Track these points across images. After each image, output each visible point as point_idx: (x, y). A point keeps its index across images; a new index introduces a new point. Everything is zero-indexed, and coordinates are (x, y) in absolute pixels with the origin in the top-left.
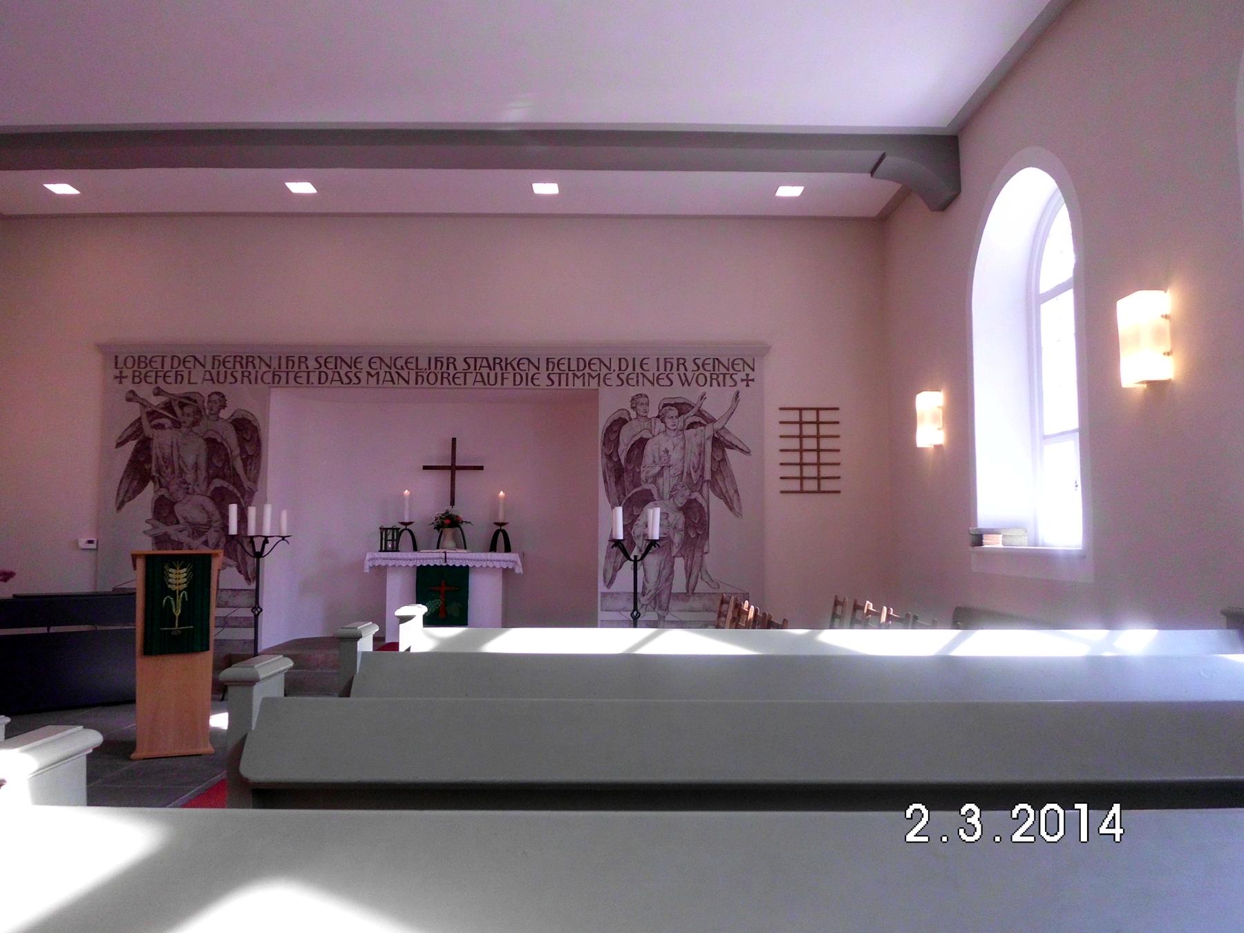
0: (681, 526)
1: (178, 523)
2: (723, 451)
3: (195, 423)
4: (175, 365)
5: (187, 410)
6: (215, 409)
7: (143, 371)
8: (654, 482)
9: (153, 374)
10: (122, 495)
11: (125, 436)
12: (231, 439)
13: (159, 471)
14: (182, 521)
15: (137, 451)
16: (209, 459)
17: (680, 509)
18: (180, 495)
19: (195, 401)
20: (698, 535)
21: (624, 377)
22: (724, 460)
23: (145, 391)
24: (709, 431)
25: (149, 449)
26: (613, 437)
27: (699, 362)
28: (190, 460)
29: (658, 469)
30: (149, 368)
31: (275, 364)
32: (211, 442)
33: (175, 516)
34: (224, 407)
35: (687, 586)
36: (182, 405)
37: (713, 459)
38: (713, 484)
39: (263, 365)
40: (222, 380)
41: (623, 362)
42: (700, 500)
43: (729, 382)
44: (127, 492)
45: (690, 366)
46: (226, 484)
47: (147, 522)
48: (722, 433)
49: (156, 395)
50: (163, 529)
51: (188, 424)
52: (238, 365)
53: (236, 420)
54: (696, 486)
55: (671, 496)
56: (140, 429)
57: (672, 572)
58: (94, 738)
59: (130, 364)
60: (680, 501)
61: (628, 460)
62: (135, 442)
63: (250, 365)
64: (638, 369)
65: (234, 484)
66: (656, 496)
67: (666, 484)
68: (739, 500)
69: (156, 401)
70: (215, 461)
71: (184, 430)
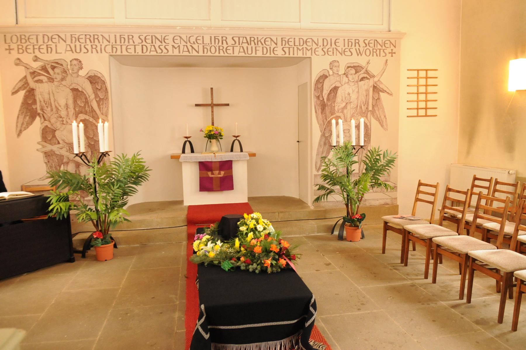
1: (59, 143)
2: (379, 93)
3: (63, 79)
4: (46, 41)
5: (56, 70)
6: (75, 71)
7: (25, 45)
8: (342, 112)
9: (31, 47)
10: (19, 125)
11: (17, 88)
12: (88, 89)
13: (42, 109)
14: (61, 142)
15: (26, 97)
16: (75, 101)
18: (58, 125)
19: (62, 65)
21: (325, 50)
22: (379, 99)
23: (27, 58)
24: (371, 82)
25: (34, 95)
27: (367, 42)
28: (62, 102)
29: (344, 104)
30: (28, 43)
31: (112, 40)
32: (75, 90)
33: (57, 139)
34: (81, 68)
36: (53, 68)
37: (373, 98)
38: (373, 112)
39: (104, 40)
40: (78, 50)
43: (382, 54)
44: (23, 124)
46: (87, 117)
47: (39, 143)
48: (378, 83)
49: (35, 61)
50: (49, 147)
51: (59, 79)
52: (88, 41)
53: (89, 77)
56: (27, 83)
59: (15, 39)
61: (328, 99)
62: (24, 92)
63: (96, 40)
64: (333, 46)
65: (93, 117)
68: (386, 121)
69: (36, 66)
70: (79, 102)
71: (56, 83)
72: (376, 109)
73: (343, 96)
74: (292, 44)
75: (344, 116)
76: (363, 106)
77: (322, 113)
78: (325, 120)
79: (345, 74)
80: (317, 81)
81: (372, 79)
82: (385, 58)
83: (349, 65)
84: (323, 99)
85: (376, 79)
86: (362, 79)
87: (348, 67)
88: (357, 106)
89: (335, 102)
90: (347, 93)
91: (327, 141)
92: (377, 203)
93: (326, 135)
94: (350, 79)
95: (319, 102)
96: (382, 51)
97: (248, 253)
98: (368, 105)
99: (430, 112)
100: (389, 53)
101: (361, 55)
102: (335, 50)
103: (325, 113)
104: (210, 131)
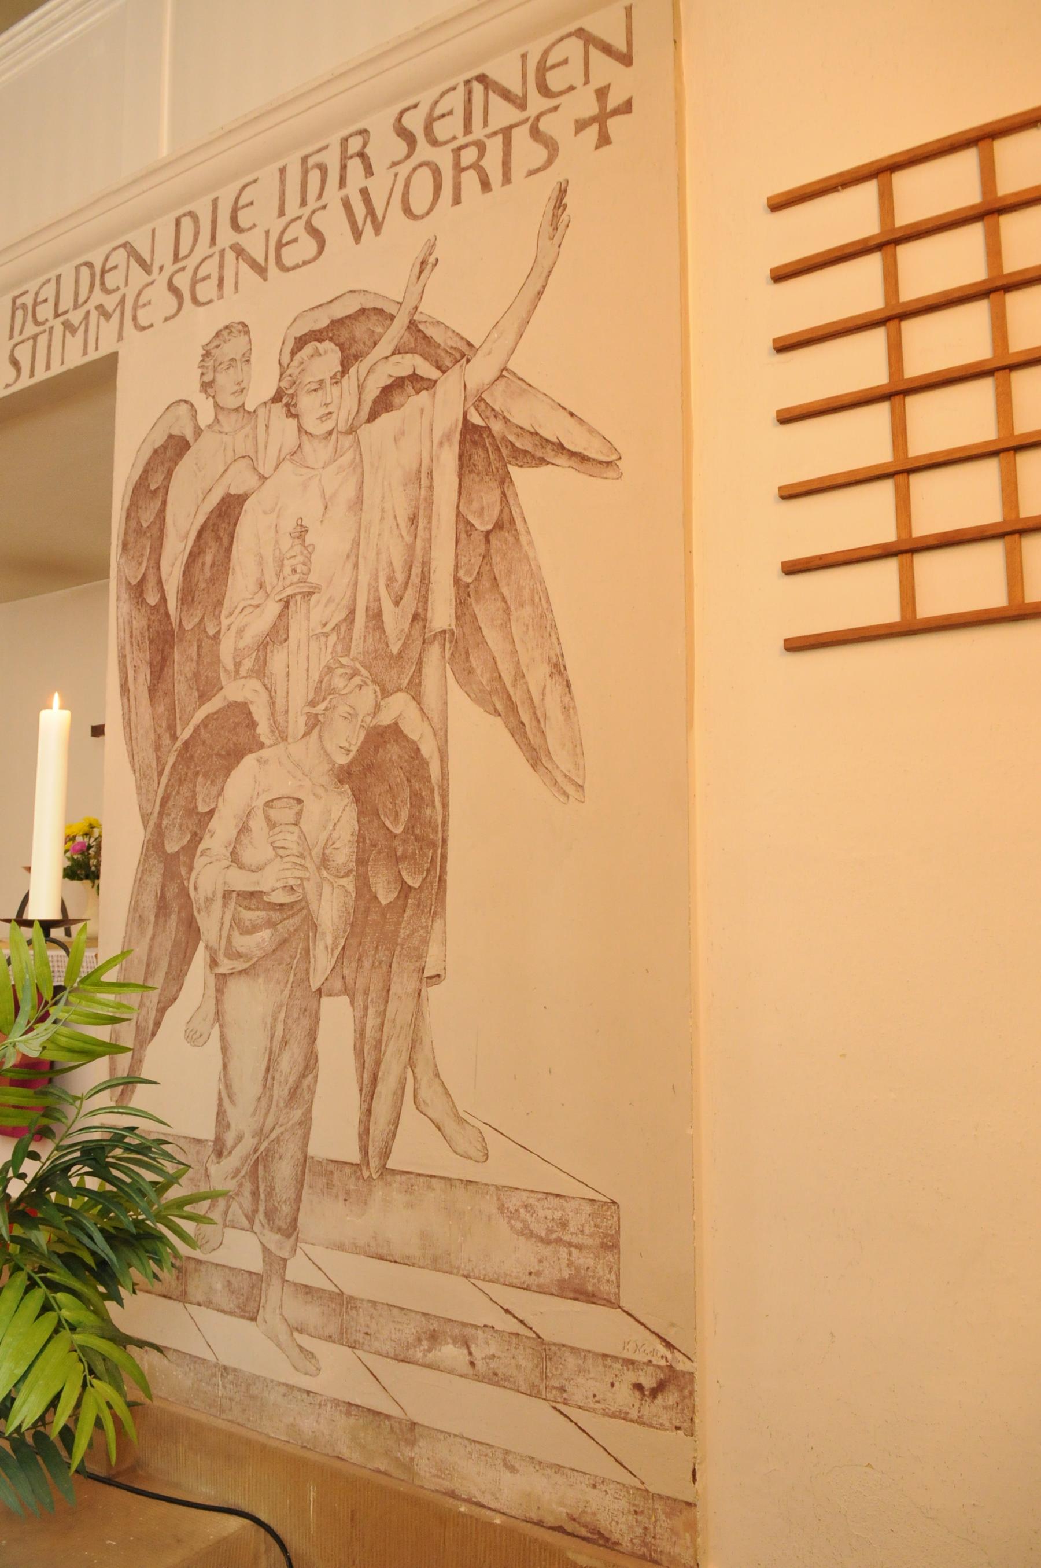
0: (343, 855)
2: (505, 480)
8: (260, 671)
20: (405, 890)
21: (182, 281)
22: (505, 523)
24: (444, 408)
26: (147, 517)
27: (414, 122)
29: (273, 609)
35: (364, 1134)
37: (464, 525)
38: (462, 643)
41: (187, 223)
42: (414, 728)
43: (527, 152)
45: (385, 147)
48: (497, 400)
54: (395, 668)
55: (314, 723)
57: (310, 1063)
60: (344, 740)
61: (187, 596)
64: (226, 236)
66: (263, 729)
67: (297, 667)
68: (568, 710)
72: (484, 611)
74: (45, 312)
75: (272, 703)
76: (387, 605)
77: (152, 691)
78: (166, 740)
79: (277, 398)
80: (136, 489)
81: (454, 374)
82: (546, 185)
83: (301, 329)
84: (164, 599)
85: (480, 371)
86: (384, 401)
87: (301, 342)
88: (352, 612)
89: (220, 603)
90: (288, 525)
91: (172, 890)
92: (504, 1491)
93: (171, 847)
94: (311, 424)
95: (140, 623)
96: (521, 136)
97: (363, 887)
98: (424, 598)
99: (855, 214)
100: (581, 126)
101: (378, 228)
102: (230, 256)
103: (170, 693)
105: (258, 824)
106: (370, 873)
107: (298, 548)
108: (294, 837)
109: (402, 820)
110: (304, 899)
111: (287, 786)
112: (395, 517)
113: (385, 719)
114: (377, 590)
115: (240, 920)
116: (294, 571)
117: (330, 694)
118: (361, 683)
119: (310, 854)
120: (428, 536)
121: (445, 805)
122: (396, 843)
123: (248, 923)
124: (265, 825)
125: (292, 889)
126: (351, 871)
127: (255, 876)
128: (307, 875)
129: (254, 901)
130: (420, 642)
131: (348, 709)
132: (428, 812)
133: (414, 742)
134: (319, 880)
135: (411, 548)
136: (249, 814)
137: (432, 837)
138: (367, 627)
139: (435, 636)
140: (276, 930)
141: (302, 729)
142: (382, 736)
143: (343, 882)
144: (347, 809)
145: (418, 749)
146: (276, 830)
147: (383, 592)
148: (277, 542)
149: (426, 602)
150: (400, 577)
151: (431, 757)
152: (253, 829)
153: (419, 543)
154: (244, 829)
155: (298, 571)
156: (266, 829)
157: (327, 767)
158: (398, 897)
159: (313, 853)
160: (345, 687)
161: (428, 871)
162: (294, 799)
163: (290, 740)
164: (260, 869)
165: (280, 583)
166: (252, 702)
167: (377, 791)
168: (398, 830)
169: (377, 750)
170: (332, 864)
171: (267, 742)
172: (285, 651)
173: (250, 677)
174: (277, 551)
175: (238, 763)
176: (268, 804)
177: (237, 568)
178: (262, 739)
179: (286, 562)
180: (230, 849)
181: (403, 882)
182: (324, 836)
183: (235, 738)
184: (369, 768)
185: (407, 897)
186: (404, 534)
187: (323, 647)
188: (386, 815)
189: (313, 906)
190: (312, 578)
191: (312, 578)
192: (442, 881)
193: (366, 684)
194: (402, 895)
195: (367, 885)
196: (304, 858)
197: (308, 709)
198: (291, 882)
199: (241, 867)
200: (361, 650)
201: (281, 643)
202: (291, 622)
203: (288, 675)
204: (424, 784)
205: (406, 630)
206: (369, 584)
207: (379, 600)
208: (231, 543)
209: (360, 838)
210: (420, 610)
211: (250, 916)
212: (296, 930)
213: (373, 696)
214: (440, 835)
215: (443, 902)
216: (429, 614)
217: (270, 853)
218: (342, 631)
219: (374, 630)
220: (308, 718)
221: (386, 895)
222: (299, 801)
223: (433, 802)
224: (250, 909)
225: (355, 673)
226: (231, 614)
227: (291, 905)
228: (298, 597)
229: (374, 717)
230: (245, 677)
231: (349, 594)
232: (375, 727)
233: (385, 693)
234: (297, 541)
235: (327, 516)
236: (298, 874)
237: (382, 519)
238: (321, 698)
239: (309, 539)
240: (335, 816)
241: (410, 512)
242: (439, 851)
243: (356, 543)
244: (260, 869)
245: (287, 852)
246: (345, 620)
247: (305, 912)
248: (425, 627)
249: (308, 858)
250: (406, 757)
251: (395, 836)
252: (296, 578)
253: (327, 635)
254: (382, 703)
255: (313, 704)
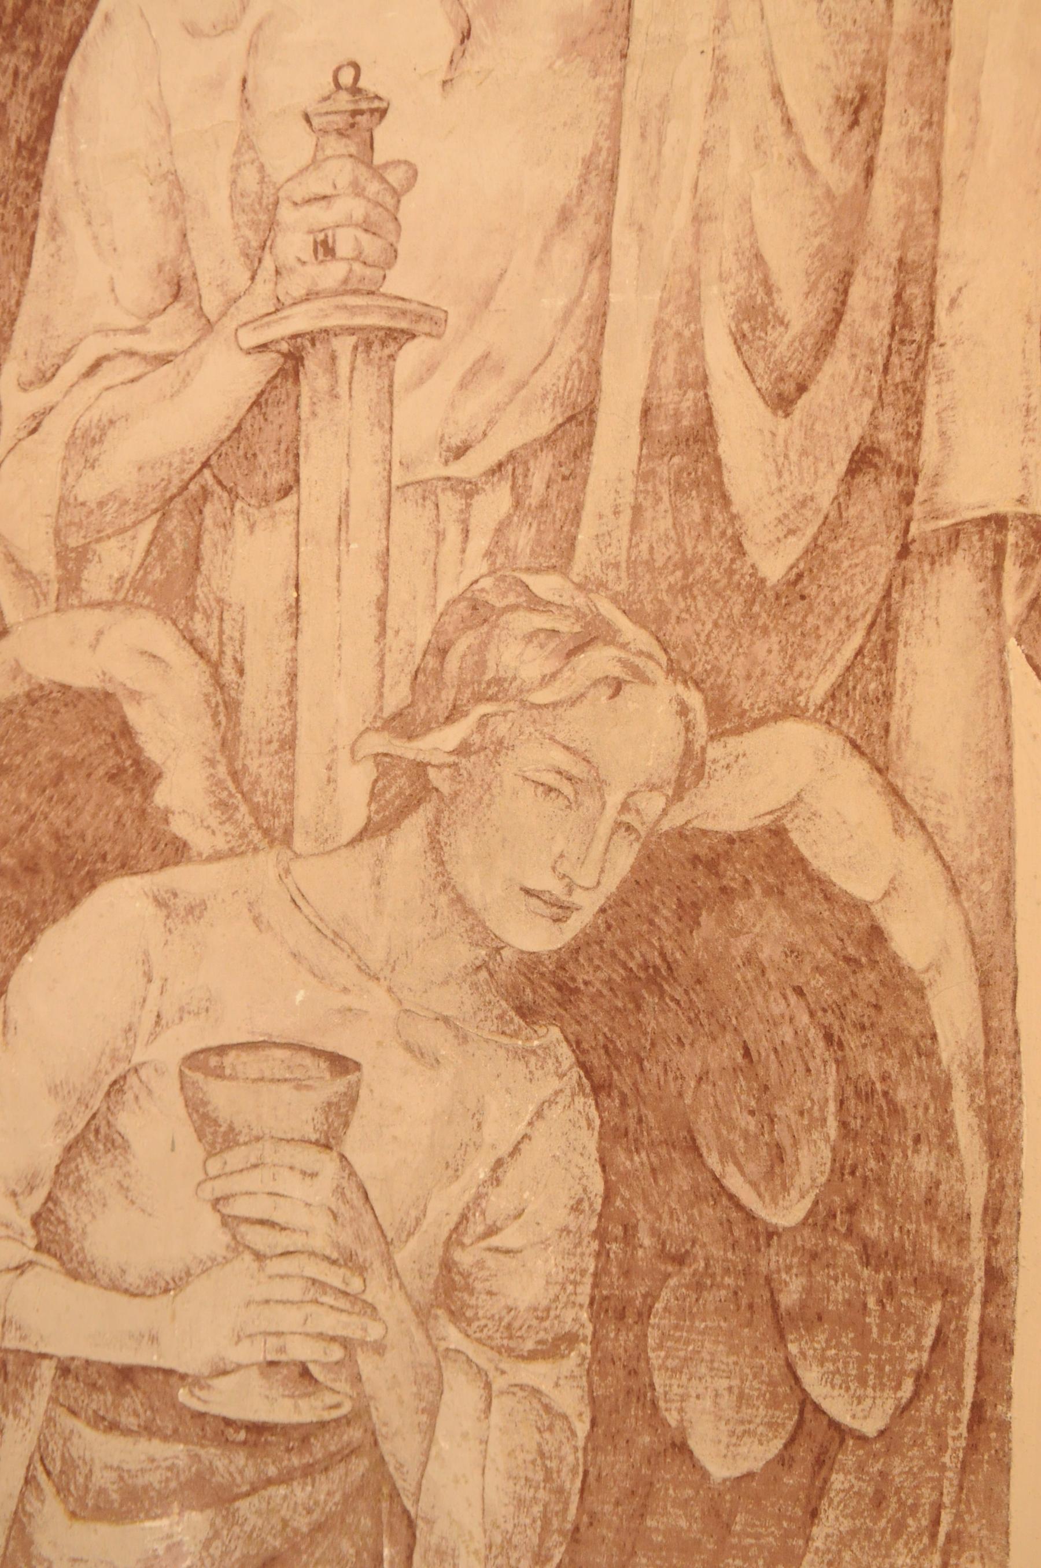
0: (536, 1271)
8: (175, 586)
17: (539, 992)
20: (816, 1440)
29: (224, 380)
42: (852, 841)
55: (404, 795)
58: (359, 1350)
60: (542, 868)
66: (183, 792)
67: (338, 595)
73: (211, 180)
75: (225, 706)
88: (580, 419)
90: (298, 81)
97: (624, 1398)
104: (280, 733)
105: (155, 1127)
106: (656, 1358)
107: (340, 171)
108: (321, 1191)
109: (802, 1180)
110: (360, 1414)
111: (296, 1007)
112: (777, 92)
113: (730, 804)
114: (693, 346)
115: (69, 1464)
116: (325, 249)
117: (479, 698)
118: (617, 671)
119: (388, 1259)
120: (925, 171)
121: (1001, 1147)
122: (772, 1259)
123: (103, 1479)
124: (186, 1133)
125: (305, 1373)
126: (571, 1339)
127: (137, 1314)
128: (375, 1332)
129: (133, 1401)
130: (886, 549)
131: (559, 757)
132: (923, 1163)
133: (858, 907)
134: (426, 1356)
135: (850, 213)
136: (117, 1087)
137: (937, 1254)
138: (644, 476)
139: (955, 534)
140: (232, 1519)
141: (355, 814)
142: (712, 867)
143: (537, 1374)
144: (554, 1113)
145: (876, 934)
146: (236, 1158)
147: (720, 354)
148: (246, 142)
149: (916, 409)
150: (798, 309)
151: (934, 966)
152: (137, 1145)
153: (884, 194)
154: (93, 1138)
155: (344, 247)
156: (192, 1149)
157: (466, 954)
158: (784, 1460)
159: (402, 1257)
160: (547, 680)
161: (923, 1378)
162: (317, 1053)
163: (299, 843)
164: (169, 1285)
165: (263, 289)
166: (135, 696)
167: (689, 1061)
168: (788, 1213)
169: (689, 913)
170: (486, 1307)
171: (200, 841)
172: (286, 530)
173: (130, 605)
174: (249, 178)
175: (74, 901)
176: (203, 1061)
177: (72, 219)
178: (180, 827)
179: (286, 214)
180: (34, 1203)
181: (806, 1405)
182: (445, 1205)
183: (58, 816)
184: (656, 977)
185: (822, 1462)
186: (818, 152)
187: (453, 534)
188: (727, 1152)
189: (401, 1449)
190: (399, 282)
191: (399, 282)
192: (987, 1422)
193: (641, 677)
194: (804, 1453)
195: (641, 1395)
196: (361, 1270)
197: (377, 742)
198: (301, 1350)
199: (78, 1270)
200: (619, 551)
201: (265, 500)
202: (309, 428)
203: (295, 612)
204: (905, 1060)
205: (825, 502)
206: (659, 325)
207: (704, 381)
208: (45, 129)
209: (612, 1226)
210: (886, 436)
211: (108, 1454)
212: (319, 1528)
213: (675, 725)
214: (977, 1252)
215: (995, 1504)
216: (929, 454)
217: (209, 1236)
218: (537, 482)
219: (678, 488)
220: (382, 774)
221: (727, 1442)
222: (340, 1064)
223: (946, 1129)
224: (113, 1427)
225: (592, 635)
226: (45, 378)
227: (303, 1435)
228: (344, 345)
229: (678, 796)
230: (108, 605)
231: (566, 349)
232: (681, 834)
233: (727, 717)
234: (334, 145)
235: (468, 64)
236: (330, 1323)
237: (716, 95)
238: (441, 710)
239: (390, 141)
240: (499, 1132)
241: (843, 77)
242: (974, 1312)
243: (603, 172)
244: (169, 1285)
245: (285, 1241)
246: (549, 441)
247: (360, 1466)
248: (908, 498)
249: (378, 1271)
250: (823, 955)
251: (772, 1233)
252: (333, 273)
253: (469, 490)
254: (714, 751)
255: (402, 724)
